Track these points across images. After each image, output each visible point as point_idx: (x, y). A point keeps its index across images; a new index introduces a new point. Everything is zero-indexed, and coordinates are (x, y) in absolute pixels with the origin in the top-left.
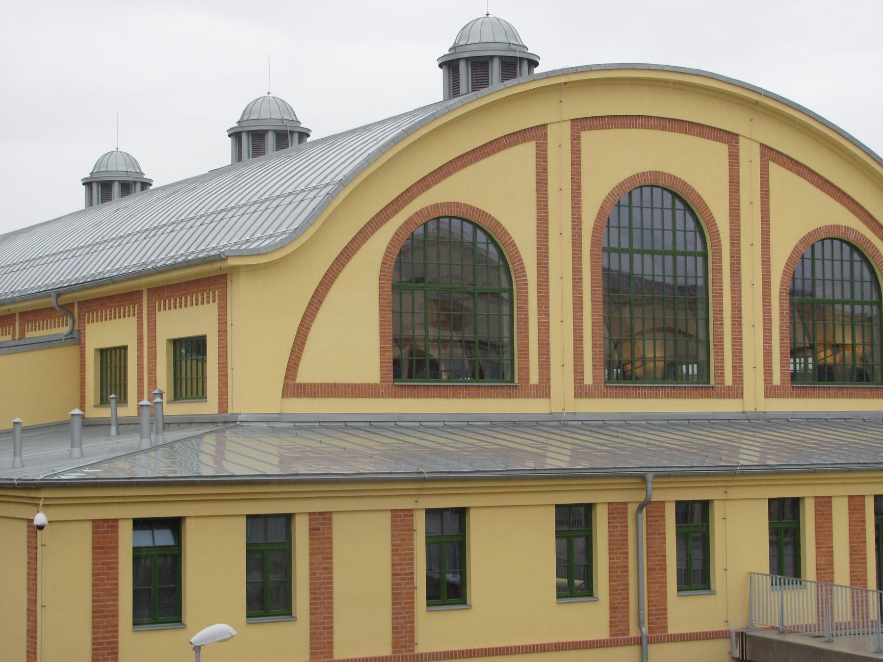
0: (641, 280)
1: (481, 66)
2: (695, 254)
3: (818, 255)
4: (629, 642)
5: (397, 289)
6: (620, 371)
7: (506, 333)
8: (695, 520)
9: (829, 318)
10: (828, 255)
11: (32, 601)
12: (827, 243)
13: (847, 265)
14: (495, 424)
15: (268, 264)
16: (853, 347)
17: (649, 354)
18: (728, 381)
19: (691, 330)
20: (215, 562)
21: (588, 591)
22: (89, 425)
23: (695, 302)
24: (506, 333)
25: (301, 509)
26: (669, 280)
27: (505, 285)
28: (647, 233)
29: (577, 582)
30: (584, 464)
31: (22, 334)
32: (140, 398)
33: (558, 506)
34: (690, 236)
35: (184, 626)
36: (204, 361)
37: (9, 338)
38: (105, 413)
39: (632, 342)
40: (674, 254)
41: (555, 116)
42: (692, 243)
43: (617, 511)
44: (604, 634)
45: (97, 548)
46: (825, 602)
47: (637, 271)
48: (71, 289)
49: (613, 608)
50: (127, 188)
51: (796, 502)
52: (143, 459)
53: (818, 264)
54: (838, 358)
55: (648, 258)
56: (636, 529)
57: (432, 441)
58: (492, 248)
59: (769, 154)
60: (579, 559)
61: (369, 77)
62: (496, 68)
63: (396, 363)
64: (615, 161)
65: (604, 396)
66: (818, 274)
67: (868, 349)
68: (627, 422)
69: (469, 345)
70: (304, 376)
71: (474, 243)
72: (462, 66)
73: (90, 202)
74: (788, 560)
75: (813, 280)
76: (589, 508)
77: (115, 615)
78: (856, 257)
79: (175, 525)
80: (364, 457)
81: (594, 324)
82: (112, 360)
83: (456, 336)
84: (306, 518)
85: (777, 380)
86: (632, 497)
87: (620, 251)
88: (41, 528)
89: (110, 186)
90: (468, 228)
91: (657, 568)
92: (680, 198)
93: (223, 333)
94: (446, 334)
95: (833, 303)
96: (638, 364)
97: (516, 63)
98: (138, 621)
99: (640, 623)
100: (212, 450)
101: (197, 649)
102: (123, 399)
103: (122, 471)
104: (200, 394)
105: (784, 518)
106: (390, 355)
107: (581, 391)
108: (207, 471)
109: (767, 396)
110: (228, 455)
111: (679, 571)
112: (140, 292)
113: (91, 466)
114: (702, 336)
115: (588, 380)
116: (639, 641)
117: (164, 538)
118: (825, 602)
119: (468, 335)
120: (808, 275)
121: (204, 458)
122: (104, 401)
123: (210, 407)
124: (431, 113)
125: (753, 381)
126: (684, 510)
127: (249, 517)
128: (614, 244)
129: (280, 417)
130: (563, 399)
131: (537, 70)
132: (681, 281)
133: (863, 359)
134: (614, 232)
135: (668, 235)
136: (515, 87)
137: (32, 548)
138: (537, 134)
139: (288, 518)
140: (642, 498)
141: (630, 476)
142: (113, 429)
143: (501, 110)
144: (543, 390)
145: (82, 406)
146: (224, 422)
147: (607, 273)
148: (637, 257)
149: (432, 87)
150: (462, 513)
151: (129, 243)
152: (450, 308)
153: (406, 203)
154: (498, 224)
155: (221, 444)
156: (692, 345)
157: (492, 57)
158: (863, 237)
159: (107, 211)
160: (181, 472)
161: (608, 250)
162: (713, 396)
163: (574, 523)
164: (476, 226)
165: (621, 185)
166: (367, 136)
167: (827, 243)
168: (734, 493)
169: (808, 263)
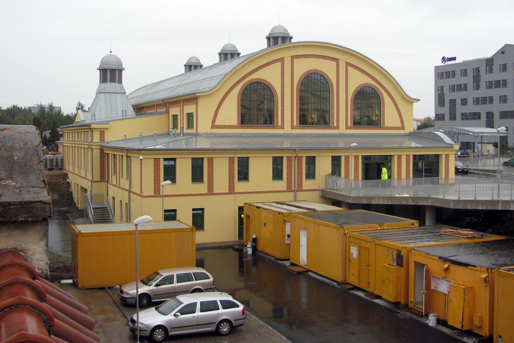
1: (278, 39)
4: (291, 191)
6: (304, 121)
7: (328, 107)
8: (311, 161)
11: (141, 177)
15: (208, 94)
18: (335, 125)
20: (184, 169)
24: (328, 107)
25: (206, 157)
43: (289, 159)
44: (285, 189)
49: (287, 183)
50: (196, 67)
52: (171, 144)
54: (377, 118)
56: (295, 163)
59: (348, 64)
64: (303, 67)
65: (300, 129)
70: (217, 123)
79: (174, 160)
80: (227, 144)
86: (293, 155)
89: (192, 67)
91: (300, 173)
93: (197, 112)
97: (286, 38)
99: (295, 186)
104: (192, 128)
105: (336, 161)
107: (293, 127)
108: (184, 147)
111: (306, 174)
116: (294, 191)
117: (172, 163)
123: (194, 131)
125: (342, 125)
126: (240, 160)
129: (211, 134)
130: (287, 129)
131: (240, 56)
137: (141, 164)
138: (282, 60)
146: (196, 135)
149: (264, 44)
150: (248, 158)
152: (256, 105)
155: (196, 139)
158: (375, 86)
163: (277, 162)
168: (321, 154)
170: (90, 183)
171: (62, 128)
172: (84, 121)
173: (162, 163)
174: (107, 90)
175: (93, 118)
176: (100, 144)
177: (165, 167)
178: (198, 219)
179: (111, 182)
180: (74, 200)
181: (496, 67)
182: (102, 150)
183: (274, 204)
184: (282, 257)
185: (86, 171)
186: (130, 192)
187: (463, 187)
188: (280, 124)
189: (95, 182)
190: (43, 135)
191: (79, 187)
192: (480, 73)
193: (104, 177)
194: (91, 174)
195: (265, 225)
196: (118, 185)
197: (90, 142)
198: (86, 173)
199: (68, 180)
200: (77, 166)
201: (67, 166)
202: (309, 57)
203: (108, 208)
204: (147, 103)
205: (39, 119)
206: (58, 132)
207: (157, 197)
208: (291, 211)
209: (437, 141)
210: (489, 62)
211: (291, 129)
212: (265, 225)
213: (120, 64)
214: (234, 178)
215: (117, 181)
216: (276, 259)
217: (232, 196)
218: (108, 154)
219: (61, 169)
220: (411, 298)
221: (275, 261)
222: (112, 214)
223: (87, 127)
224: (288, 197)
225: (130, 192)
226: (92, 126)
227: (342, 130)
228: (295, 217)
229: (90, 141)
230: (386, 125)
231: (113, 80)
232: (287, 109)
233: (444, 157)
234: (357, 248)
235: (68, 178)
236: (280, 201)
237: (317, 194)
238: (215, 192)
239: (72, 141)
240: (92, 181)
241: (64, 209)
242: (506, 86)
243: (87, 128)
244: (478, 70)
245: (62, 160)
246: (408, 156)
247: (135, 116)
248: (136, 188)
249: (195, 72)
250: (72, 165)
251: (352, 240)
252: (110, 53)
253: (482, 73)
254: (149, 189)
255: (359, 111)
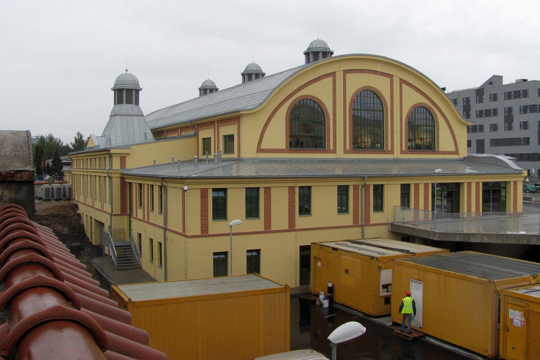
0: (364, 118)
1: (317, 54)
2: (380, 111)
3: (416, 111)
4: (359, 226)
5: (291, 121)
6: (357, 146)
7: (323, 134)
8: (379, 190)
9: (419, 130)
10: (419, 112)
11: (184, 212)
12: (419, 108)
13: (425, 115)
14: (320, 161)
15: (252, 113)
16: (426, 139)
17: (366, 141)
19: (379, 134)
20: (236, 201)
21: (347, 211)
22: (200, 160)
23: (380, 125)
24: (323, 134)
25: (262, 186)
26: (372, 119)
27: (323, 119)
28: (366, 104)
29: (344, 208)
30: (347, 174)
31: (181, 133)
32: (215, 153)
33: (338, 186)
34: (379, 105)
35: (227, 220)
36: (233, 142)
37: (177, 135)
38: (204, 157)
39: (361, 136)
40: (374, 111)
41: (339, 69)
42: (379, 107)
43: (356, 187)
45: (202, 197)
46: (416, 215)
47: (363, 116)
48: (195, 120)
49: (354, 216)
50: (211, 91)
51: (409, 185)
52: (215, 171)
53: (416, 114)
55: (366, 112)
56: (361, 193)
57: (301, 166)
58: (319, 108)
59: (402, 81)
60: (344, 202)
61: (283, 58)
62: (321, 55)
63: (291, 143)
65: (353, 153)
66: (417, 117)
67: (431, 140)
68: (359, 161)
69: (312, 137)
70: (263, 146)
71: (314, 107)
72: (311, 54)
73: (201, 95)
74: (406, 202)
75: (415, 119)
76: (347, 186)
77: (207, 216)
78: (428, 112)
79: (225, 190)
80: (281, 171)
81: (350, 132)
82: (207, 142)
83: (308, 135)
84: (263, 189)
85: (404, 149)
86: (360, 183)
87: (357, 110)
88: (186, 191)
89: (207, 90)
90: (312, 102)
91: (367, 204)
92: (375, 94)
93: (239, 133)
94: (305, 134)
95: (421, 126)
96: (363, 143)
97: (327, 53)
98: (214, 218)
99: (362, 221)
100: (236, 169)
101: (231, 227)
102: (210, 153)
103: (209, 174)
104: (232, 152)
105: (405, 189)
106: (289, 140)
107: (346, 152)
108: (234, 175)
109: (401, 153)
110: (240, 170)
112: (215, 121)
113: (200, 173)
114: (382, 135)
115: (348, 148)
116: (362, 226)
117: (221, 194)
118: (416, 215)
119: (312, 135)
120: (413, 117)
121: (233, 171)
122: (204, 154)
123: (235, 155)
124: (301, 68)
127: (246, 188)
128: (356, 108)
129: (256, 159)
130: (340, 154)
131: (333, 56)
132: (376, 119)
133: (429, 142)
134: (356, 104)
135: (372, 105)
136: (326, 60)
137: (183, 197)
138: (333, 75)
139: (258, 189)
140: (363, 183)
141: (360, 177)
142: (207, 162)
143: (322, 67)
144: (334, 151)
145: (198, 155)
146: (239, 160)
147: (354, 116)
148: (363, 112)
149: (301, 61)
150: (310, 188)
151: (213, 107)
152: (306, 127)
153: (294, 95)
154: (321, 101)
156: (379, 138)
157: (320, 52)
159: (205, 98)
160: (227, 175)
161: (354, 109)
162: (385, 153)
163: (343, 191)
164: (314, 102)
165: (358, 90)
166: (282, 75)
167: (419, 108)
168: (390, 182)
169: (413, 114)
170: (109, 216)
171: (70, 155)
172: (99, 146)
173: (211, 194)
174: (123, 112)
175: (109, 143)
176: (121, 171)
177: (215, 199)
178: (254, 262)
179: (135, 215)
180: (87, 234)
181: (486, 97)
182: (123, 179)
183: (349, 244)
184: (376, 313)
185: (103, 202)
186: (165, 229)
187: (531, 216)
188: (332, 148)
189: (115, 215)
190: (46, 164)
191: (93, 219)
192: (470, 103)
193: (126, 209)
194: (110, 206)
195: (347, 271)
196: (146, 219)
197: (109, 169)
198: (102, 205)
199: (78, 212)
200: (89, 196)
201: (76, 196)
202: (362, 72)
203: (132, 246)
204: (169, 126)
205: (41, 148)
206: (61, 161)
207: (205, 236)
208: (384, 254)
209: (501, 166)
210: (479, 92)
211: (344, 153)
212: (347, 271)
213: (137, 83)
214: (294, 212)
215: (144, 215)
216: (365, 314)
217: (293, 234)
218: (130, 183)
219: (69, 199)
220: (501, 353)
221: (366, 318)
222: (138, 254)
223: (106, 153)
224: (355, 234)
225: (165, 229)
226: (112, 151)
227: (397, 154)
228: (402, 264)
229: (108, 168)
230: (441, 149)
231: (129, 101)
232: (339, 130)
233: (512, 184)
234: (522, 313)
235: (78, 209)
236: (351, 239)
237: (385, 229)
238: (273, 229)
239: (83, 169)
240: (111, 215)
241: (75, 244)
242: (496, 115)
243: (105, 153)
244: (468, 100)
245: (70, 189)
246: (477, 184)
247: (154, 140)
248: (175, 223)
249: (212, 94)
250: (84, 195)
251: (510, 300)
252: (126, 72)
253: (473, 103)
254: (194, 227)
255: (372, 138)
